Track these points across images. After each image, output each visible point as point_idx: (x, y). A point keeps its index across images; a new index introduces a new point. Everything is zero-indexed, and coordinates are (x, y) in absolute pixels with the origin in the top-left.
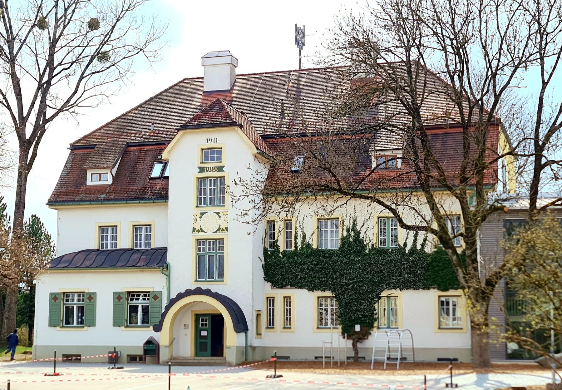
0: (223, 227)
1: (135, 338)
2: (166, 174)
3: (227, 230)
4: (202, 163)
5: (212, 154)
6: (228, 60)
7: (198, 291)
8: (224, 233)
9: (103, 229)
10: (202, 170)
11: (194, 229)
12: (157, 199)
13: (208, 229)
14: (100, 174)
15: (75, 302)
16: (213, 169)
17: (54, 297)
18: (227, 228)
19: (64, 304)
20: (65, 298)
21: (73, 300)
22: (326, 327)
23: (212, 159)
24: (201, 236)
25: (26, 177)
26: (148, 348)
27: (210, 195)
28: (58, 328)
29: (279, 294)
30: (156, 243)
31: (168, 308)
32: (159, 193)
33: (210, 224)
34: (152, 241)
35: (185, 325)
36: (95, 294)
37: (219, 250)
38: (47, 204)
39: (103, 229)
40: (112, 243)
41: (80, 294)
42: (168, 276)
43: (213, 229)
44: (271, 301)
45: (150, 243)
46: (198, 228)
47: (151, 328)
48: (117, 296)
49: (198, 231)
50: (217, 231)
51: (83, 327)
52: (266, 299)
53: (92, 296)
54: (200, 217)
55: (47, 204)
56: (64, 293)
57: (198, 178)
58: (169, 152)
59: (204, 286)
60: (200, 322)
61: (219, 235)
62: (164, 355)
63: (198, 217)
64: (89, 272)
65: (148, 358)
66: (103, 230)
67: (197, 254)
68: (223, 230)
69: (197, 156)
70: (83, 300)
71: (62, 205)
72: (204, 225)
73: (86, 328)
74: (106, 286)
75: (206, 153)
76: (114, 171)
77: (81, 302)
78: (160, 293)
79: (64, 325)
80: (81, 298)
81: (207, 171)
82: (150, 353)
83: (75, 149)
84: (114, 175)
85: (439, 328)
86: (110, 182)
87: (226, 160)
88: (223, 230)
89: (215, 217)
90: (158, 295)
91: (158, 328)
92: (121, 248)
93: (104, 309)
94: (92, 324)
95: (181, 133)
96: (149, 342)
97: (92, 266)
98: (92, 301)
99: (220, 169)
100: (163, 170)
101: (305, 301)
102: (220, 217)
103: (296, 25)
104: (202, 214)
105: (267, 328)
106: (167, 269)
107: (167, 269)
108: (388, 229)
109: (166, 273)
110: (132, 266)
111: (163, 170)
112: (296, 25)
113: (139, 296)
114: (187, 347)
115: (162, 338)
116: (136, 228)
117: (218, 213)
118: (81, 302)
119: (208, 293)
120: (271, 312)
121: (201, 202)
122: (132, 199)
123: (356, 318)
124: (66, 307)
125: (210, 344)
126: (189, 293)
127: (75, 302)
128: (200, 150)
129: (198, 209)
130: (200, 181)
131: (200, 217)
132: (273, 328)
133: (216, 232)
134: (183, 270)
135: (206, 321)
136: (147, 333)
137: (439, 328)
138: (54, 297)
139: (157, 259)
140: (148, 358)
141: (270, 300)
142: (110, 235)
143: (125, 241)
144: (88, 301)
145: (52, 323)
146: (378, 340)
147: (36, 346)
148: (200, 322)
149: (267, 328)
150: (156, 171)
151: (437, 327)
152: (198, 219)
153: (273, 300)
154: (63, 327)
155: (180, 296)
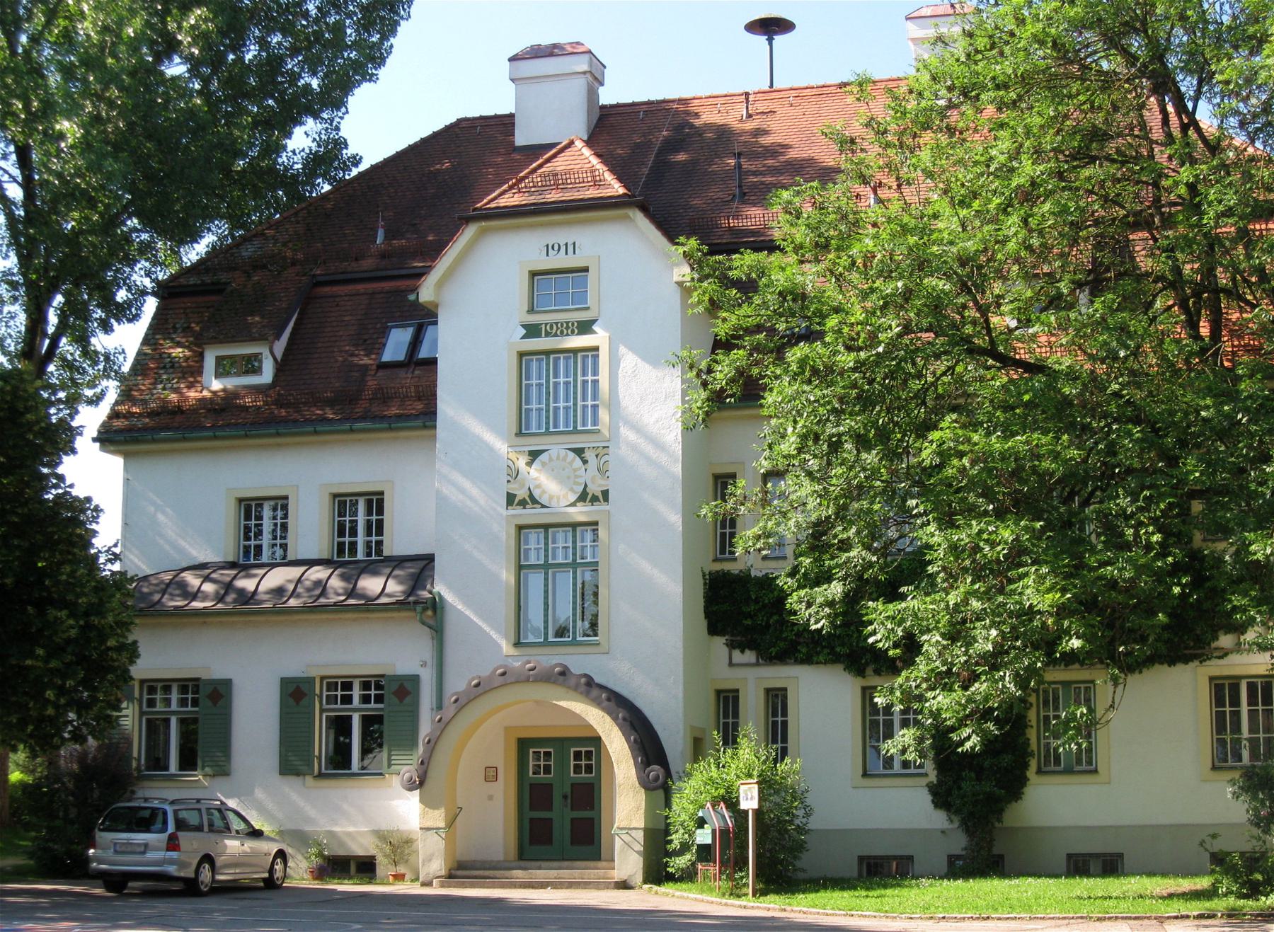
0: (595, 489)
2: (423, 353)
3: (606, 499)
8: (596, 507)
9: (249, 508)
11: (510, 499)
13: (564, 459)
15: (174, 706)
18: (605, 494)
19: (322, 711)
20: (146, 697)
21: (168, 702)
22: (1057, 768)
24: (530, 515)
32: (404, 400)
34: (290, 540)
38: (94, 440)
39: (249, 508)
46: (522, 494)
49: (523, 503)
52: (712, 697)
55: (94, 440)
57: (521, 355)
58: (440, 284)
60: (572, 763)
66: (342, 505)
68: (595, 499)
70: (195, 703)
72: (551, 459)
76: (280, 346)
77: (372, 705)
78: (415, 679)
79: (323, 770)
80: (373, 692)
81: (548, 334)
84: (279, 357)
87: (605, 293)
90: (408, 686)
92: (395, 554)
98: (408, 700)
100: (416, 343)
109: (431, 622)
111: (416, 343)
113: (167, 689)
116: (342, 503)
117: (579, 452)
118: (372, 705)
124: (148, 721)
127: (174, 706)
132: (1095, 771)
137: (865, 774)
141: (726, 699)
142: (361, 518)
144: (209, 703)
148: (572, 763)
150: (396, 344)
151: (860, 772)
153: (736, 699)
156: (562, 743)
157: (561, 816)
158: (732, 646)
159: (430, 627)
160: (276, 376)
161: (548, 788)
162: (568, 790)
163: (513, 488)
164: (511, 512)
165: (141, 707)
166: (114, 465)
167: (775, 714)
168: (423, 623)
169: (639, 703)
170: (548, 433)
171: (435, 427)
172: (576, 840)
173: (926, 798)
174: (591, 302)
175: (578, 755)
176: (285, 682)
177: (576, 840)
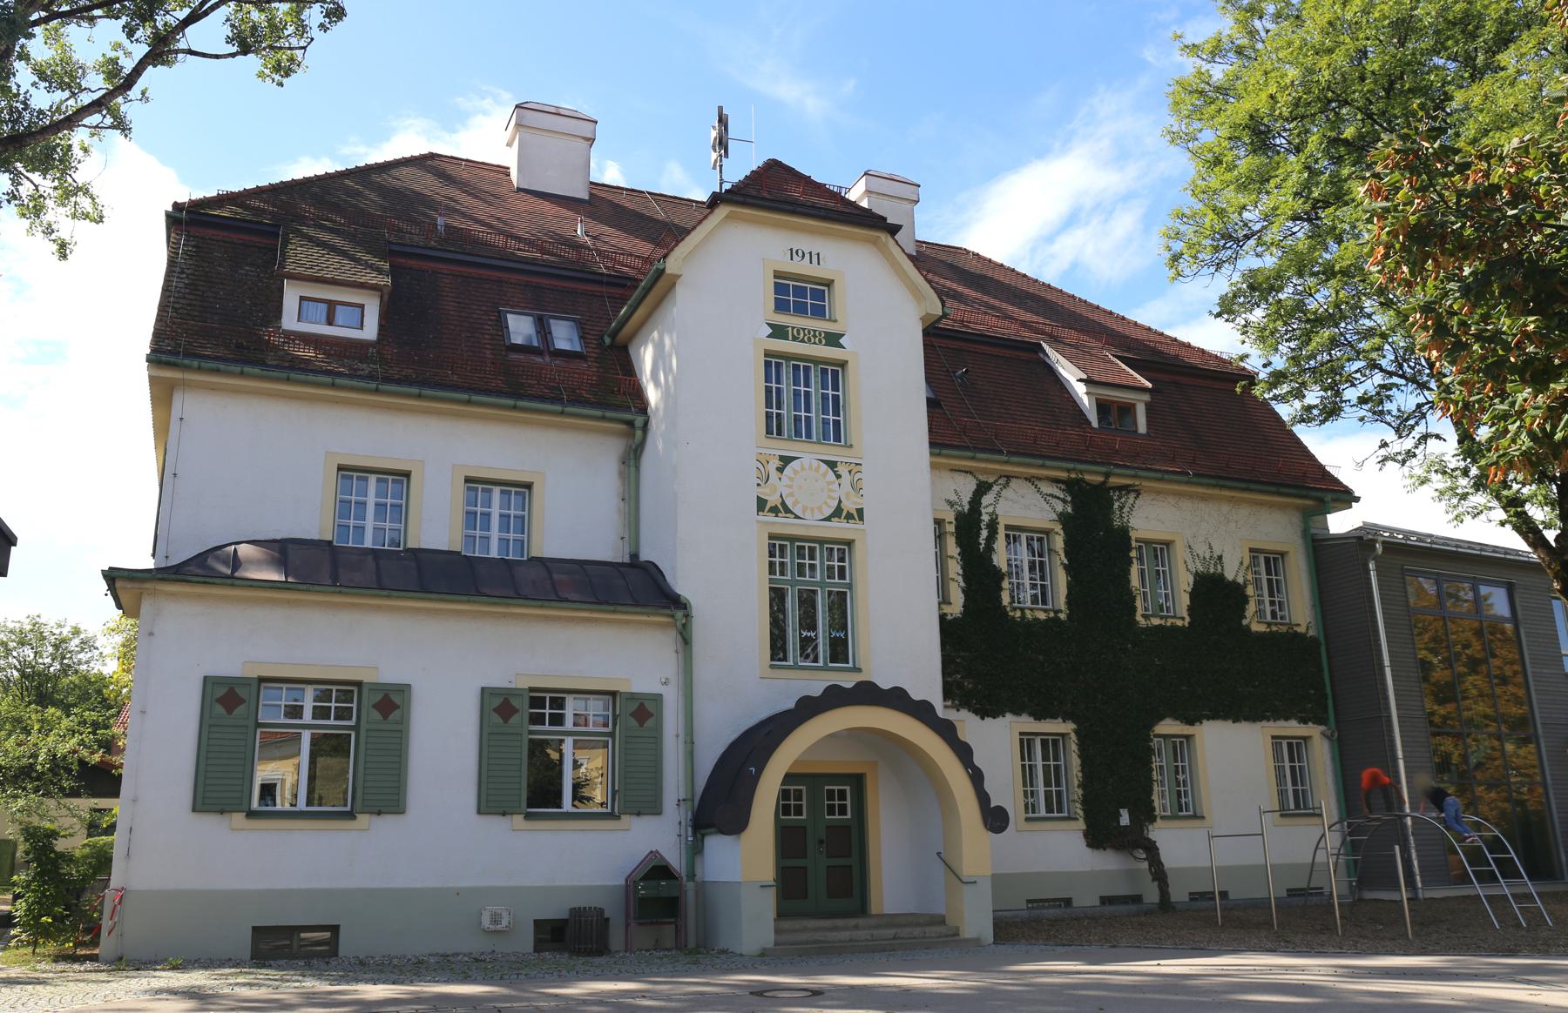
0: (849, 506)
1: (583, 858)
3: (861, 518)
8: (851, 525)
11: (761, 504)
13: (805, 509)
15: (307, 717)
16: (811, 337)
18: (860, 512)
36: (404, 690)
37: (801, 574)
41: (325, 688)
42: (686, 639)
46: (773, 500)
49: (774, 510)
53: (396, 699)
54: (780, 470)
57: (767, 354)
61: (839, 529)
68: (849, 517)
71: (217, 371)
72: (791, 494)
73: (363, 819)
74: (446, 668)
78: (657, 699)
81: (795, 338)
89: (824, 475)
90: (650, 706)
93: (444, 746)
99: (833, 340)
102: (839, 477)
103: (720, 109)
104: (786, 460)
112: (720, 109)
117: (832, 465)
121: (773, 427)
123: (1118, 795)
127: (307, 717)
130: (773, 364)
133: (828, 519)
139: (633, 587)
143: (436, 525)
148: (848, 802)
152: (774, 474)
163: (764, 492)
164: (761, 518)
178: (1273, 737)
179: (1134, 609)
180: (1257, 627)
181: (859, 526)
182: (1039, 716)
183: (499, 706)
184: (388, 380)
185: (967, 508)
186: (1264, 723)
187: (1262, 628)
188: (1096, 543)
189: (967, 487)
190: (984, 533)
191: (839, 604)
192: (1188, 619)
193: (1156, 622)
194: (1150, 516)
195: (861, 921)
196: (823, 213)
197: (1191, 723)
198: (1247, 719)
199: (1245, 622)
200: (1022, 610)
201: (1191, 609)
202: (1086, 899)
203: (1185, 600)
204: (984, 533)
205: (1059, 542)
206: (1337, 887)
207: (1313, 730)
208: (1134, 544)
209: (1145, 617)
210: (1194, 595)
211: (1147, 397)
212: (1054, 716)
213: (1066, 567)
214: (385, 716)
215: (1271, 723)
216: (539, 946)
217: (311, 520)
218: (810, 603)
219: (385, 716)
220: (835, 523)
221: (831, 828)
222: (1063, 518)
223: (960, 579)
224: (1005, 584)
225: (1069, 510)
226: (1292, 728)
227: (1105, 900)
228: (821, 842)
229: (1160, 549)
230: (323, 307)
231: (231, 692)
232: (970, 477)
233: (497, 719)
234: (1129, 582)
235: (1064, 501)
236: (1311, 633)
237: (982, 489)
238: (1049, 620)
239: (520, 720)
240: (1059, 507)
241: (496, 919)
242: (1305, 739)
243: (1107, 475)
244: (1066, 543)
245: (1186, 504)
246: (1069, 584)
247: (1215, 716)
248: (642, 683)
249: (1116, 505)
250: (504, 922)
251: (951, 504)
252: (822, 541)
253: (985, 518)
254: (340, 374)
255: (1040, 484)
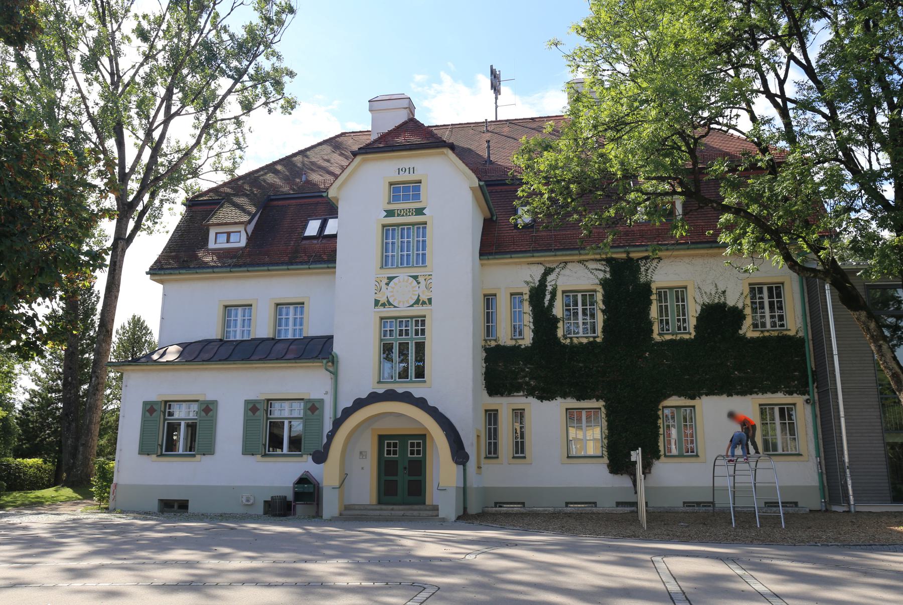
0: (424, 298)
1: (281, 473)
3: (430, 303)
4: (389, 203)
5: (405, 189)
6: (405, 103)
7: (391, 396)
8: (425, 307)
10: (390, 213)
11: (377, 302)
12: (315, 262)
13: (399, 302)
14: (229, 234)
17: (150, 408)
18: (430, 300)
19: (165, 420)
23: (406, 198)
25: (123, 251)
26: (301, 490)
27: (408, 242)
28: (154, 456)
29: (505, 405)
30: (313, 329)
31: (337, 423)
33: (403, 294)
35: (361, 453)
36: (215, 403)
38: (147, 273)
40: (244, 320)
42: (335, 374)
43: (407, 301)
44: (492, 416)
45: (301, 330)
46: (383, 300)
47: (310, 458)
48: (250, 406)
49: (384, 305)
50: (415, 303)
51: (194, 456)
53: (211, 407)
54: (387, 284)
55: (147, 273)
56: (166, 402)
57: (384, 226)
59: (400, 388)
61: (418, 310)
62: (330, 504)
63: (383, 284)
64: (206, 369)
65: (300, 508)
67: (381, 340)
68: (424, 303)
69: (383, 193)
71: (171, 274)
72: (393, 296)
73: (198, 457)
74: (232, 391)
75: (396, 190)
78: (321, 401)
81: (398, 215)
82: (303, 500)
83: (193, 205)
85: (568, 457)
86: (243, 243)
87: (429, 198)
88: (424, 303)
90: (317, 405)
91: (320, 457)
93: (230, 427)
94: (209, 450)
95: (359, 159)
96: (304, 480)
97: (214, 359)
98: (210, 414)
99: (420, 212)
101: (546, 416)
102: (419, 283)
103: (492, 66)
104: (390, 279)
105: (486, 458)
106: (333, 363)
107: (333, 363)
108: (672, 306)
109: (331, 369)
110: (277, 359)
112: (492, 66)
114: (365, 487)
115: (327, 474)
117: (415, 277)
119: (407, 398)
120: (493, 434)
121: (385, 263)
122: (277, 264)
124: (168, 423)
125: (401, 485)
126: (374, 398)
128: (387, 185)
129: (383, 271)
131: (387, 284)
133: (412, 306)
134: (360, 365)
135: (395, 445)
136: (305, 465)
138: (150, 408)
140: (300, 508)
143: (262, 328)
145: (145, 449)
146: (673, 477)
147: (116, 484)
149: (486, 458)
152: (384, 287)
154: (162, 455)
155: (359, 404)
156: (403, 438)
157: (402, 479)
158: (725, 304)
159: (331, 372)
160: (247, 243)
161: (394, 463)
162: (406, 464)
163: (378, 297)
164: (377, 310)
165: (164, 416)
166: (156, 289)
167: (490, 424)
168: (327, 370)
169: (448, 415)
170: (397, 267)
171: (335, 268)
172: (410, 493)
173: (605, 470)
174: (423, 197)
175: (412, 445)
176: (247, 402)
177: (410, 493)
178: (760, 405)
179: (652, 331)
180: (751, 334)
181: (429, 307)
182: (579, 398)
183: (252, 407)
184: (235, 266)
185: (537, 284)
186: (754, 396)
187: (756, 334)
188: (626, 294)
189: (540, 270)
190: (548, 297)
191: (420, 348)
192: (694, 334)
193: (668, 337)
194: (664, 273)
195: (422, 507)
196: (408, 147)
197: (693, 398)
198: (737, 394)
199: (741, 332)
200: (571, 338)
201: (696, 327)
202: (607, 505)
203: (693, 322)
204: (548, 297)
205: (599, 297)
206: (815, 502)
207: (798, 400)
208: (654, 291)
209: (659, 334)
210: (699, 319)
211: (682, 198)
212: (590, 398)
213: (603, 311)
214: (207, 414)
215: (760, 395)
216: (266, 513)
217: (212, 331)
218: (405, 348)
219: (207, 414)
220: (416, 307)
221: (411, 462)
222: (604, 283)
223: (531, 325)
224: (560, 325)
225: (608, 276)
226: (780, 398)
227: (618, 504)
228: (405, 468)
229: (680, 293)
230: (225, 235)
231: (152, 407)
232: (541, 266)
233: (250, 413)
234: (648, 314)
235: (605, 272)
236: (801, 334)
237: (548, 272)
238: (590, 343)
239: (260, 414)
240: (601, 275)
241: (248, 501)
242: (794, 404)
243: (628, 253)
244: (603, 296)
245: (699, 262)
246: (604, 322)
247: (709, 393)
248: (315, 395)
249: (643, 269)
250: (251, 501)
251: (527, 283)
252: (412, 317)
253: (549, 288)
254: (217, 267)
255: (587, 264)
